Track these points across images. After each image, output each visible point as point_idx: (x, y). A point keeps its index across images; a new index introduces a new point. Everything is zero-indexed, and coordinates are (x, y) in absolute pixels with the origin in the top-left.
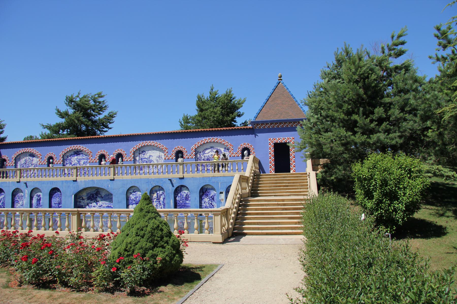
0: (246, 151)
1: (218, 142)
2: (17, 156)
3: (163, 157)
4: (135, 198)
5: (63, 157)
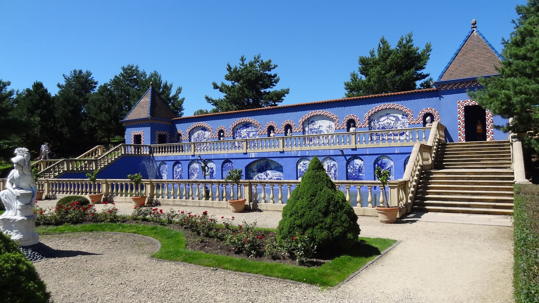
0: (429, 117)
1: (394, 108)
2: (191, 130)
3: (334, 127)
4: (305, 170)
5: (233, 130)
